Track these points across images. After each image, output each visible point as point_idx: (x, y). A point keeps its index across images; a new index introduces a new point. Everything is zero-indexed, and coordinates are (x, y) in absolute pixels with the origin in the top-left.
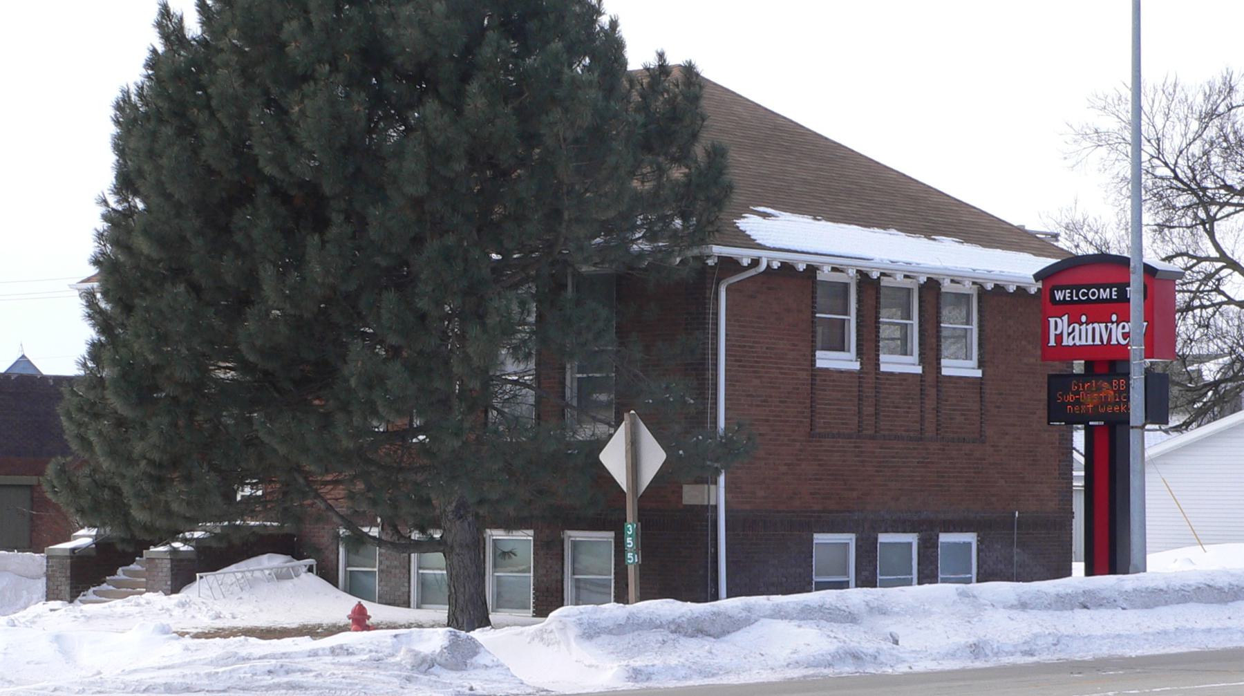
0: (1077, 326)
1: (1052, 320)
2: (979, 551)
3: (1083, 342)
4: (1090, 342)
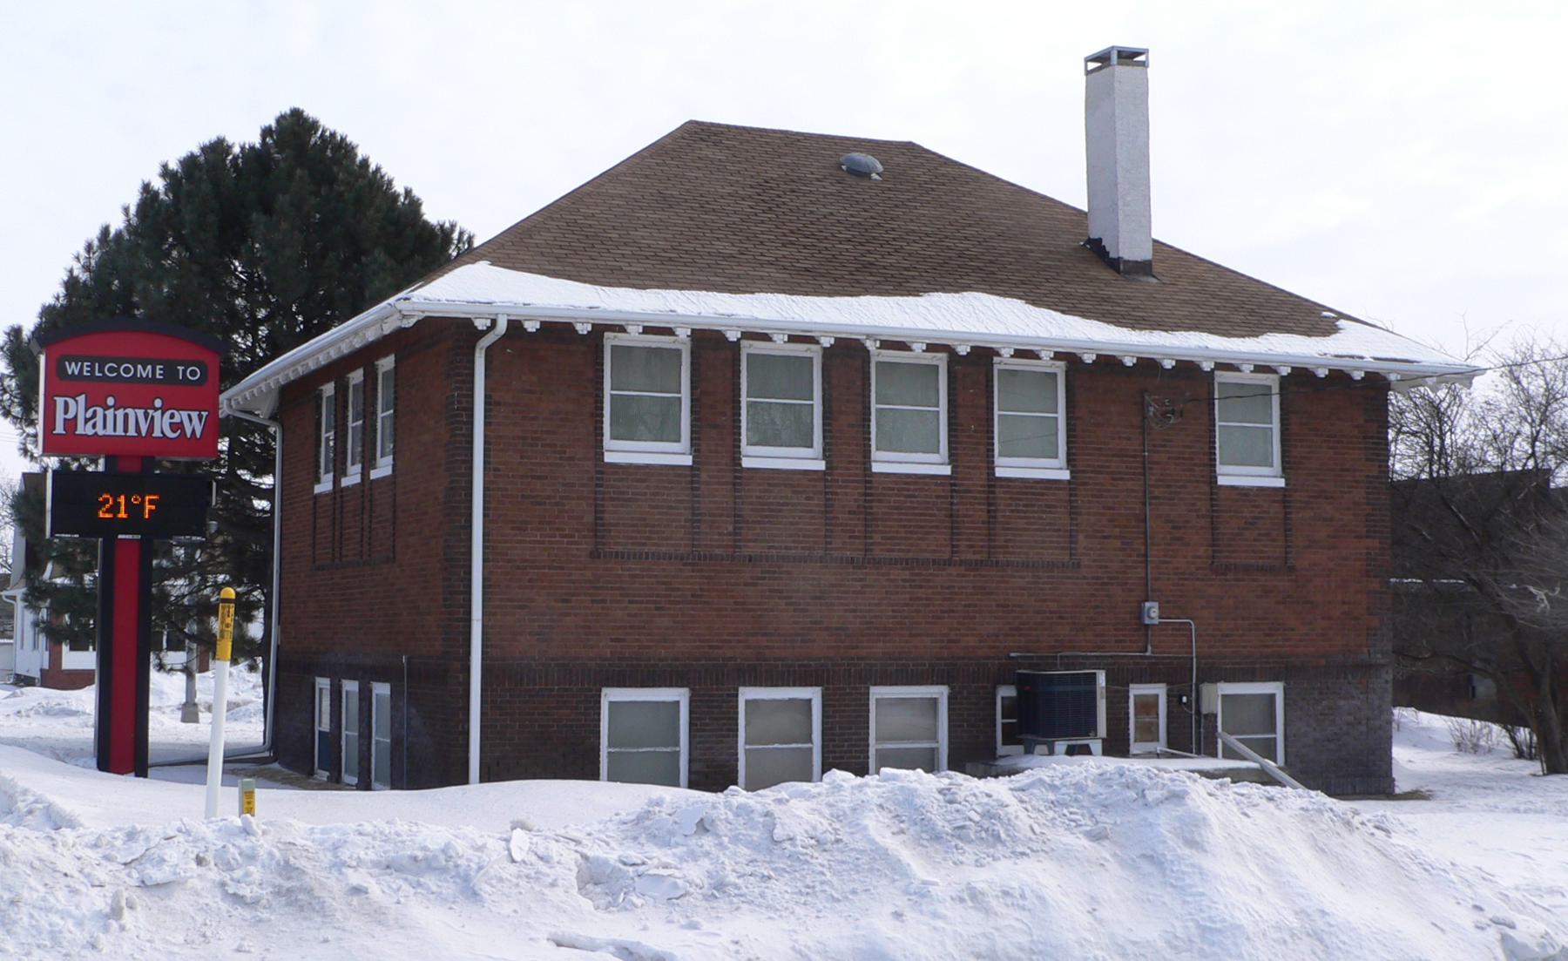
3: (110, 431)
4: (120, 432)
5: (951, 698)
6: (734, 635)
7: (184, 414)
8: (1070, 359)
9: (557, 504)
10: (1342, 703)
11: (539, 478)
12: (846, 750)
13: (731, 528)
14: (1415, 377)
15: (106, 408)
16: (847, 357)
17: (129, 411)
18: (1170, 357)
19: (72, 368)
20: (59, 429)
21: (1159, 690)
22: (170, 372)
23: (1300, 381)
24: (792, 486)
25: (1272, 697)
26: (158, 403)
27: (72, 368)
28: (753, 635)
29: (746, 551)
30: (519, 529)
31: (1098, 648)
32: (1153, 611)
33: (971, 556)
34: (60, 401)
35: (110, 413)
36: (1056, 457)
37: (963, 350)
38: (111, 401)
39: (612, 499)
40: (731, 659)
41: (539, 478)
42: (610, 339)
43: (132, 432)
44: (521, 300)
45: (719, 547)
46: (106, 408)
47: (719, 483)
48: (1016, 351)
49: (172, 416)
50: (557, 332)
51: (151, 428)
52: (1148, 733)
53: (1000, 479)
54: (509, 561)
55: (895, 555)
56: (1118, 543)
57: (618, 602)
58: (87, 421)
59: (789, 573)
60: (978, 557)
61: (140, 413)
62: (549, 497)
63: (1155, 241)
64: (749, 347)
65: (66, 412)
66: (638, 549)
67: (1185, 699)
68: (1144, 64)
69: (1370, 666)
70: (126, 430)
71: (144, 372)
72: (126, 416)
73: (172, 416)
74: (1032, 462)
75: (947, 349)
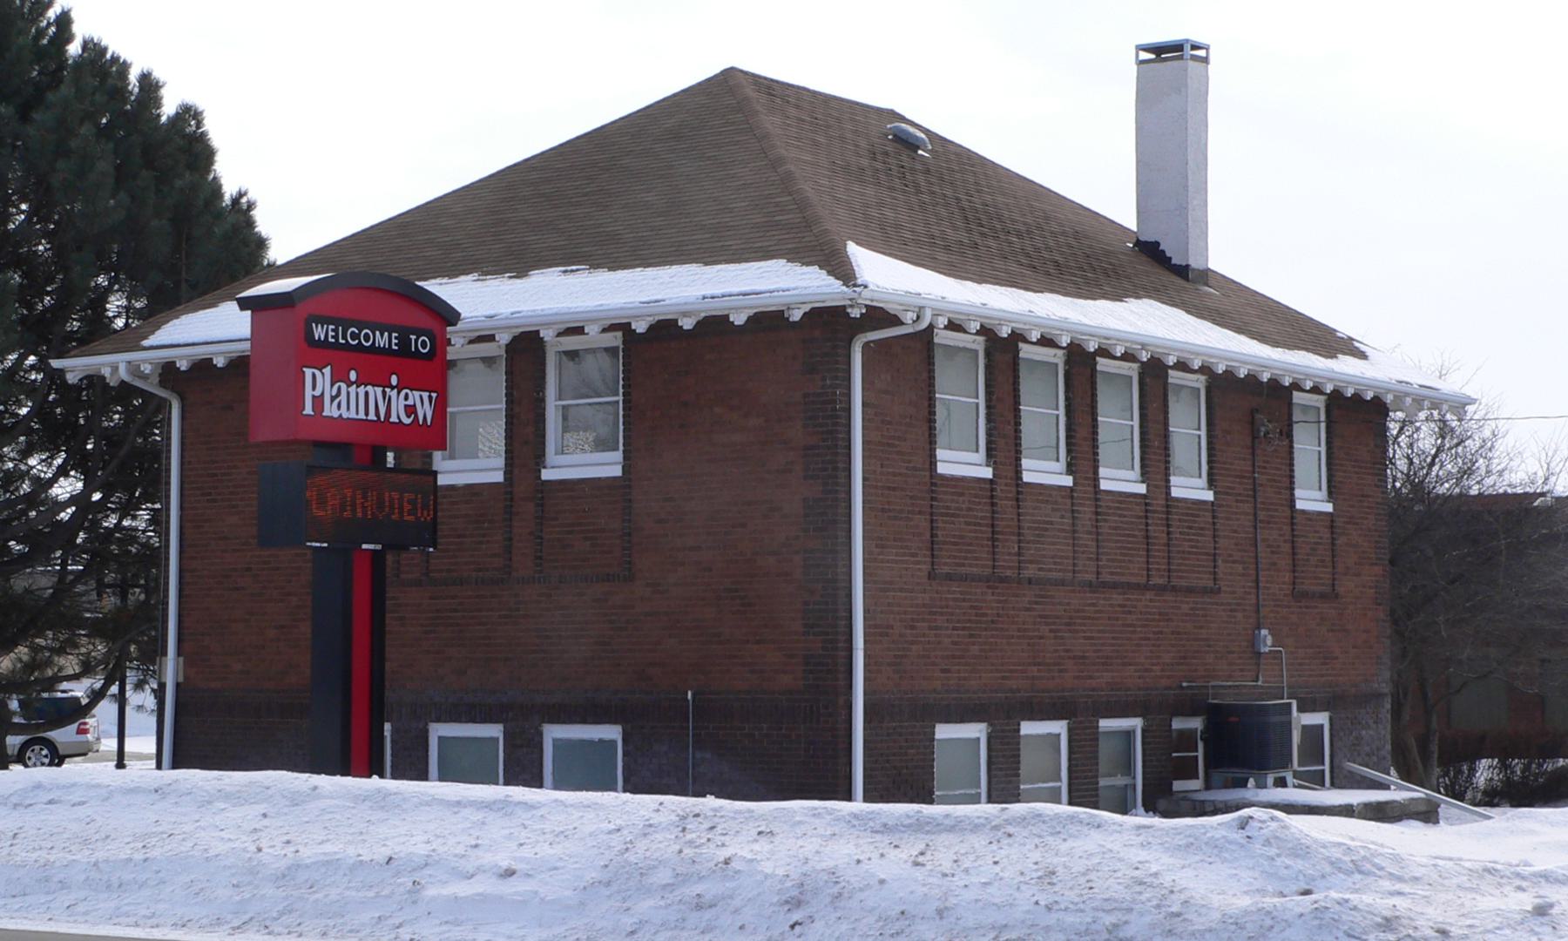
0: (343, 386)
1: (308, 372)
2: (1070, 741)
3: (353, 415)
4: (362, 416)
5: (1070, 730)
7: (417, 394)
12: (1004, 787)
14: (1400, 397)
15: (349, 384)
17: (369, 388)
19: (319, 332)
22: (404, 342)
37: (640, 327)
43: (372, 416)
49: (406, 398)
58: (333, 399)
65: (314, 388)
68: (1205, 60)
70: (367, 414)
72: (367, 394)
73: (406, 398)
74: (580, 459)
75: (625, 328)
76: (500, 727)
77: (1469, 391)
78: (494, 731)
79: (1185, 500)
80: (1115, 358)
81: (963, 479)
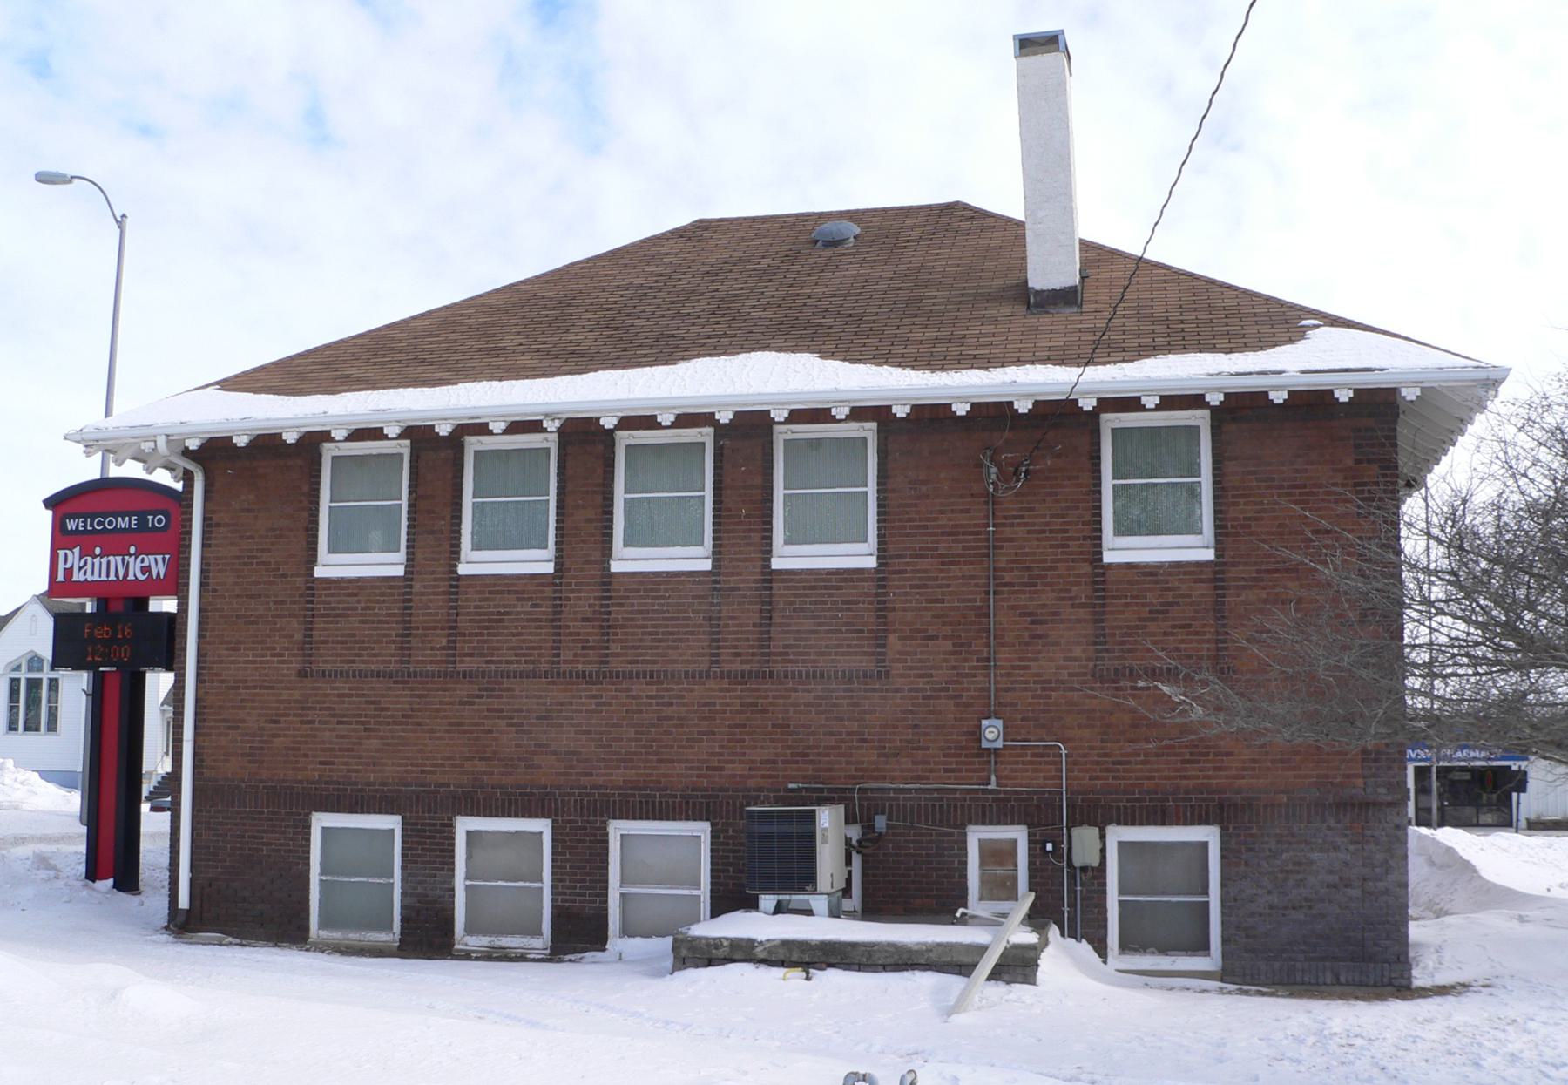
3: (96, 578)
4: (104, 577)
5: (714, 836)
6: (449, 758)
8: (878, 414)
9: (267, 623)
10: (1315, 856)
11: (252, 597)
13: (444, 642)
16: (585, 440)
18: (962, 399)
19: (71, 525)
20: (60, 578)
21: (1018, 834)
22: (142, 522)
23: (1241, 412)
24: (516, 592)
25: (1204, 846)
26: (132, 550)
27: (71, 525)
28: (467, 759)
29: (461, 667)
30: (233, 649)
31: (917, 779)
32: (992, 731)
33: (738, 667)
34: (61, 553)
35: (97, 560)
36: (865, 541)
38: (98, 551)
39: (323, 616)
40: (442, 785)
41: (252, 597)
42: (473, 444)
43: (112, 577)
44: (177, 420)
45: (431, 662)
46: (94, 557)
47: (434, 594)
48: (853, 409)
50: (267, 444)
51: (126, 573)
52: (1001, 888)
53: (780, 572)
54: (223, 681)
55: (635, 668)
56: (948, 645)
57: (326, 723)
59: (508, 689)
60: (747, 667)
61: (119, 559)
62: (261, 616)
63: (1086, 246)
64: (624, 438)
66: (346, 667)
67: (1049, 847)
69: (1366, 805)
71: (123, 523)
76: (398, 818)
77: (1491, 355)
78: (391, 822)
79: (1119, 566)
80: (840, 421)
81: (1160, 565)
